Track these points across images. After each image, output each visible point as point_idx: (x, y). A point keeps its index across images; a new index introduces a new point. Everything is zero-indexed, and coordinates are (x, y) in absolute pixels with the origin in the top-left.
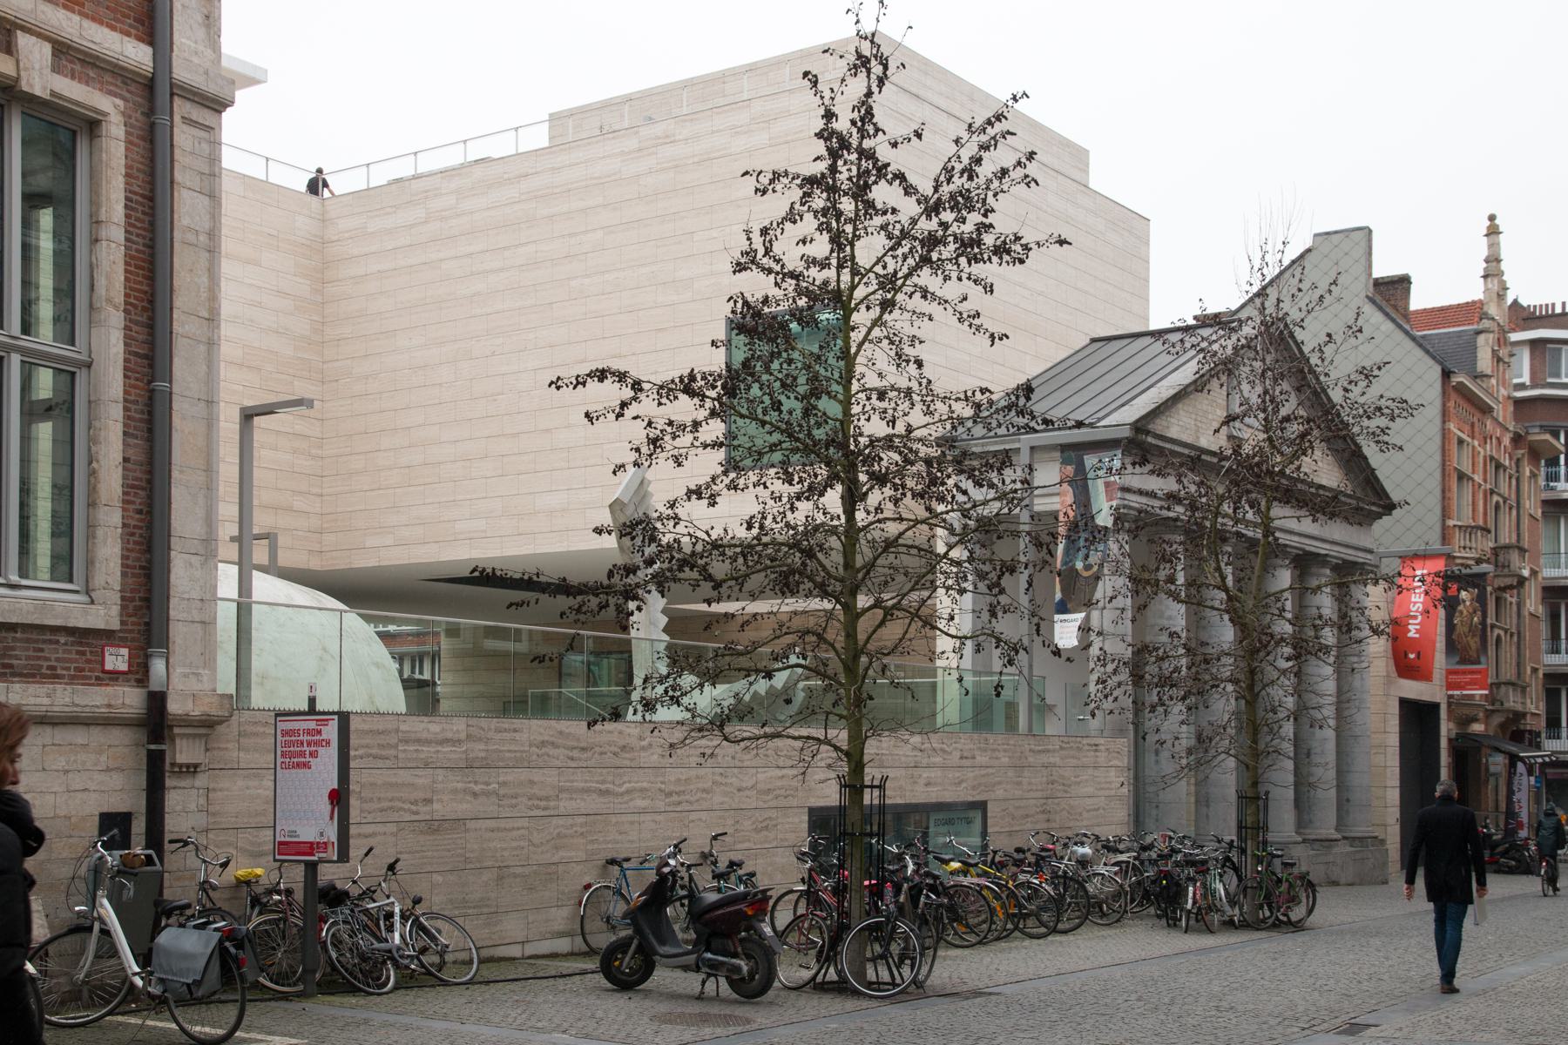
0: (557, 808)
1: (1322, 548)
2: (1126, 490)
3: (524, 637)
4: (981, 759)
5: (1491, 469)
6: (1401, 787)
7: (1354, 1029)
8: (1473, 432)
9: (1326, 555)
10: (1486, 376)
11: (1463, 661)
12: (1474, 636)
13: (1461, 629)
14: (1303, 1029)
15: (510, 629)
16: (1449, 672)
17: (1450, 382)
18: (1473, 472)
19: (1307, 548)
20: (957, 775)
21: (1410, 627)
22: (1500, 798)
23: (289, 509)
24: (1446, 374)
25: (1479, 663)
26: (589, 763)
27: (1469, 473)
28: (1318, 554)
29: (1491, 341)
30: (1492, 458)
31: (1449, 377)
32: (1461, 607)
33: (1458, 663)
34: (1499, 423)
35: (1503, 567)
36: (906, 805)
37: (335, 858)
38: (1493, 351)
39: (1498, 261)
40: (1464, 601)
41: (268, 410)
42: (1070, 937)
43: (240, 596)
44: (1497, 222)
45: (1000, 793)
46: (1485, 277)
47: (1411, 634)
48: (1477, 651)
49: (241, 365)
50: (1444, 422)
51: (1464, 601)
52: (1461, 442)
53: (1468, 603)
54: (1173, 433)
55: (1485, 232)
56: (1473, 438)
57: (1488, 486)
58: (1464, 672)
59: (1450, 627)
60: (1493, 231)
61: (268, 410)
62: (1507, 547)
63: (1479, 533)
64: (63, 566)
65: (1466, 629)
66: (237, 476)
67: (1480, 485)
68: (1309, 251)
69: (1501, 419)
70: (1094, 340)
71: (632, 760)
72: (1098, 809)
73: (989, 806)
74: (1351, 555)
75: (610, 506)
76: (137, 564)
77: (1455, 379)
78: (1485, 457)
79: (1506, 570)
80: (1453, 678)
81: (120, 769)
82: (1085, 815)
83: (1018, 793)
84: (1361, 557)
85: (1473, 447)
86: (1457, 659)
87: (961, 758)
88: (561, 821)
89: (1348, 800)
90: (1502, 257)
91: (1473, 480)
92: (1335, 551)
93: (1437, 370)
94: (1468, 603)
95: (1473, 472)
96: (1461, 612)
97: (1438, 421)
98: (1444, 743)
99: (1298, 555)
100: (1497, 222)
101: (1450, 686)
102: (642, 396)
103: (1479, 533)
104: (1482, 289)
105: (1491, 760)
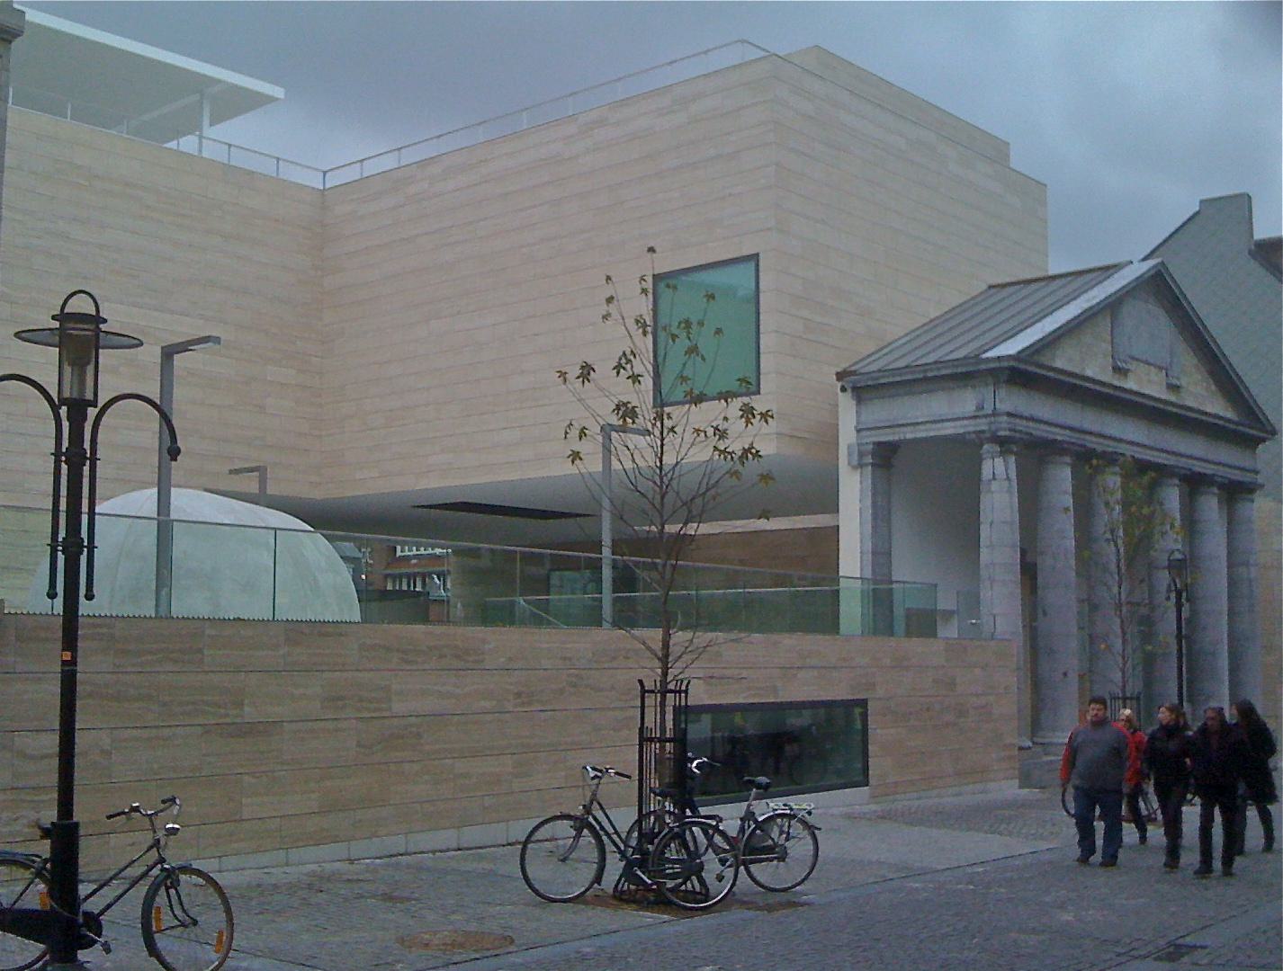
0: (390, 709)
1: (1208, 469)
2: (374, 881)
7: (1175, 952)
9: (1214, 475)
14: (1119, 955)
15: (579, 557)
26: (426, 666)
41: (184, 347)
43: (158, 515)
54: (1059, 364)
61: (184, 347)
68: (1197, 213)
70: (991, 287)
71: (476, 662)
74: (1236, 475)
81: (1205, 521)
84: (1247, 478)
88: (395, 721)
92: (1221, 471)
99: (1185, 475)
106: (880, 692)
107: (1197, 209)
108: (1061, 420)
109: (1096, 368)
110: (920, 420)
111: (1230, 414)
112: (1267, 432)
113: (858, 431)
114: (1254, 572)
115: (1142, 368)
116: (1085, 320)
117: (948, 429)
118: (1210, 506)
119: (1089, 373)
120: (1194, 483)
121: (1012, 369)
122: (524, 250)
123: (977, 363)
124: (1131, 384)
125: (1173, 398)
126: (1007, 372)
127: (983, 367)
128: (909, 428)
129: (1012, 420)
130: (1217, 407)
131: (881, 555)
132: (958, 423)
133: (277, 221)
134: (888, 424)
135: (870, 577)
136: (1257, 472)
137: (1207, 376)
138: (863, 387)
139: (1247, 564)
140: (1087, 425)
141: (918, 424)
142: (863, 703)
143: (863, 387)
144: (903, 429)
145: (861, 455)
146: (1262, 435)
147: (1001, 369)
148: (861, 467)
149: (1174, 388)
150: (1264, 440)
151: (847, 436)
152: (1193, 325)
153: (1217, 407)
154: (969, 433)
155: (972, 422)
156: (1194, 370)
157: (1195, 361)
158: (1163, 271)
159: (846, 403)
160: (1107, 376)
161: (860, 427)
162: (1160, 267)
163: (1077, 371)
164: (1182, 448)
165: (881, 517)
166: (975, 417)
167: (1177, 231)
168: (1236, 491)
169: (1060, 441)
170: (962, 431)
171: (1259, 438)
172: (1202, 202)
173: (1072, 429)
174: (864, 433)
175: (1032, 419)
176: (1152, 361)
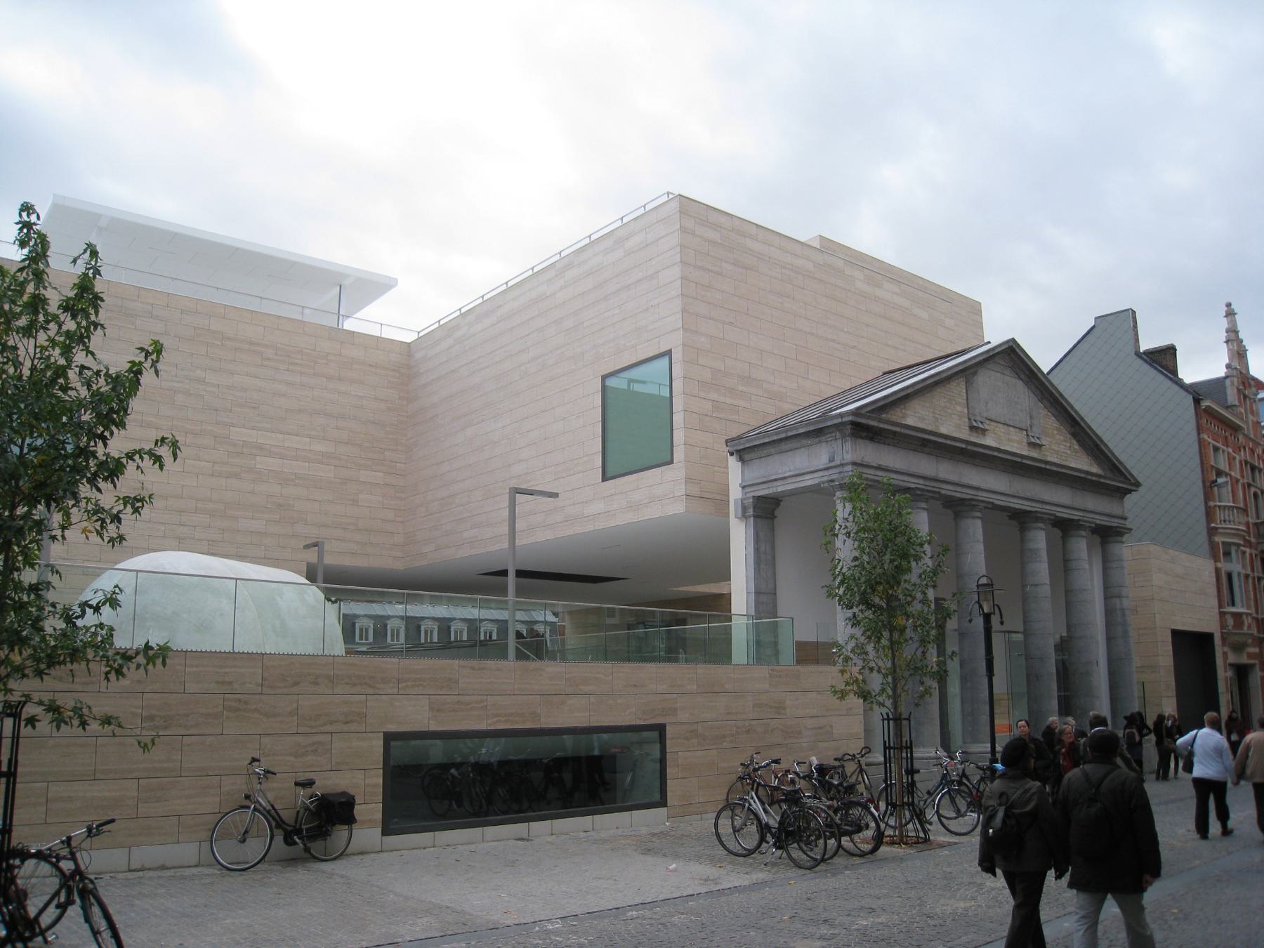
5: (1248, 471)
6: (1177, 696)
8: (1227, 442)
9: (1079, 520)
10: (1235, 406)
18: (1230, 469)
19: (1058, 514)
24: (1197, 401)
27: (1227, 470)
29: (1236, 384)
30: (1246, 462)
31: (1199, 403)
34: (1250, 439)
38: (1239, 390)
39: (1236, 332)
44: (1232, 307)
46: (1227, 342)
50: (1199, 434)
52: (1216, 449)
54: (910, 421)
55: (1225, 314)
56: (1227, 446)
57: (1245, 481)
60: (1230, 314)
63: (1235, 511)
64: (1229, 576)
67: (1237, 481)
69: (1252, 436)
74: (1105, 521)
75: (671, 462)
76: (130, 482)
77: (1205, 404)
84: (1115, 523)
85: (1228, 453)
90: (1239, 328)
91: (1231, 476)
93: (1190, 399)
97: (1195, 433)
103: (1235, 511)
106: (683, 716)
107: (1093, 324)
108: (913, 470)
109: (952, 426)
110: (787, 475)
111: (1095, 469)
112: (1132, 484)
113: (743, 488)
114: (1126, 603)
115: (1001, 429)
116: (937, 383)
117: (809, 481)
118: (1080, 546)
119: (943, 430)
120: (1065, 527)
121: (853, 423)
122: (523, 368)
123: (825, 420)
124: (989, 441)
125: (1034, 454)
126: (850, 426)
127: (829, 423)
128: (779, 483)
129: (860, 469)
130: (1082, 463)
131: (766, 598)
132: (816, 475)
133: (370, 365)
134: (764, 480)
135: (754, 614)
136: (1125, 519)
137: (1069, 436)
138: (745, 450)
139: (1120, 597)
140: (943, 475)
141: (784, 478)
142: (661, 729)
143: (745, 450)
144: (775, 484)
145: (744, 509)
146: (1129, 487)
147: (842, 424)
148: (746, 518)
149: (1033, 445)
150: (1130, 491)
151: (735, 493)
152: (1051, 394)
153: (1082, 463)
154: (823, 483)
155: (826, 473)
156: (1055, 432)
157: (1056, 424)
158: (1014, 346)
159: (734, 464)
160: (964, 434)
161: (744, 484)
162: (1011, 344)
163: (929, 428)
164: (1047, 497)
165: (764, 560)
166: (827, 469)
167: (1079, 342)
168: (1107, 534)
169: (913, 488)
170: (816, 481)
171: (1126, 489)
172: (1096, 318)
173: (924, 478)
174: (747, 490)
175: (879, 468)
176: (1011, 423)
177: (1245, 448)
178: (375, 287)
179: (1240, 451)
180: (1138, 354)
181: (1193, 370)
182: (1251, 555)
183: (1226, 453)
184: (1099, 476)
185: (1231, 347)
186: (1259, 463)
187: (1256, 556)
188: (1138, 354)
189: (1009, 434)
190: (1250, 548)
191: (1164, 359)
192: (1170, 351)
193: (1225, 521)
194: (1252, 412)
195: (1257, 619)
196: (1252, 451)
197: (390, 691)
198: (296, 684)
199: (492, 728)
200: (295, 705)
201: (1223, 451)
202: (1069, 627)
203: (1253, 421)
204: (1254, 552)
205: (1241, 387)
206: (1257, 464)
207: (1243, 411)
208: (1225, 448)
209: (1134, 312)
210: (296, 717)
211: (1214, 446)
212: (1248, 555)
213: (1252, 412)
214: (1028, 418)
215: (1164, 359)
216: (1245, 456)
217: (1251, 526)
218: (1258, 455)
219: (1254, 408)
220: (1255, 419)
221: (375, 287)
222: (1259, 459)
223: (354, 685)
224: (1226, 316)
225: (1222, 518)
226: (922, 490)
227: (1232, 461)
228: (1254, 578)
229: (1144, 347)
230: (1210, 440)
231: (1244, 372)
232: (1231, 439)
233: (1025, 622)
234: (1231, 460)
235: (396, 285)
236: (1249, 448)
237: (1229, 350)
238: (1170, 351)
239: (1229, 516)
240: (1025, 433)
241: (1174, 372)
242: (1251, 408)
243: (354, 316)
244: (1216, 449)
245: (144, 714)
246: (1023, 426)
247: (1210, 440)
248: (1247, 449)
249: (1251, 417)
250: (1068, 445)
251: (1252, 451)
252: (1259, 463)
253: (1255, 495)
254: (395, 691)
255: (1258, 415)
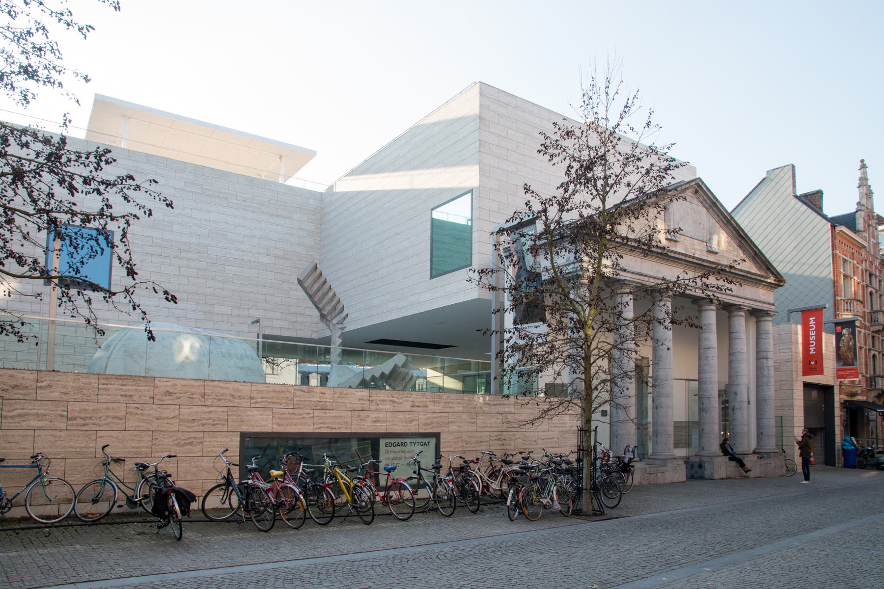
3: (473, 366)
4: (431, 407)
9: (740, 305)
10: (861, 231)
11: (845, 364)
12: (850, 352)
13: (843, 349)
16: (838, 370)
17: (835, 231)
20: (407, 416)
21: (811, 349)
22: (878, 432)
23: (304, 314)
25: (853, 365)
28: (736, 305)
31: (835, 228)
32: (843, 338)
33: (843, 365)
35: (875, 321)
36: (351, 433)
37: (383, 442)
39: (866, 179)
40: (844, 335)
42: (444, 520)
44: (865, 163)
45: (454, 428)
47: (811, 353)
48: (852, 359)
49: (282, 258)
51: (844, 335)
52: (845, 261)
53: (846, 336)
55: (859, 168)
56: (853, 259)
58: (846, 370)
59: (838, 348)
60: (863, 166)
62: (877, 312)
65: (846, 348)
66: (113, 270)
72: (553, 438)
73: (442, 436)
78: (862, 270)
79: (876, 323)
80: (840, 373)
82: (539, 441)
83: (472, 428)
84: (766, 307)
85: (854, 264)
86: (842, 363)
87: (413, 406)
89: (762, 433)
94: (846, 336)
95: (854, 276)
96: (843, 341)
98: (837, 405)
100: (865, 163)
101: (839, 377)
102: (682, 324)
104: (858, 192)
105: (870, 413)
118: (740, 322)
125: (711, 258)
177: (866, 260)
178: (304, 156)
179: (862, 263)
180: (796, 197)
181: (833, 207)
182: (865, 334)
183: (852, 264)
184: (759, 275)
185: (861, 191)
186: (875, 271)
187: (868, 334)
188: (796, 197)
189: (694, 245)
190: (865, 329)
191: (813, 200)
192: (819, 194)
193: (847, 310)
194: (874, 237)
195: (866, 377)
196: (871, 263)
197: (244, 405)
198: (192, 394)
199: (317, 431)
200: (177, 412)
201: (850, 263)
202: (730, 377)
203: (873, 243)
204: (867, 332)
205: (867, 219)
206: (874, 272)
207: (867, 235)
208: (851, 260)
209: (793, 167)
210: (178, 420)
211: (843, 259)
212: (862, 334)
213: (874, 237)
214: (708, 234)
215: (813, 200)
216: (866, 266)
217: (866, 314)
218: (875, 266)
219: (875, 234)
220: (875, 241)
221: (304, 156)
222: (876, 269)
223: (220, 400)
224: (859, 187)
225: (846, 308)
226: (630, 281)
227: (855, 269)
228: (866, 350)
229: (799, 193)
230: (840, 255)
231: (869, 207)
232: (856, 255)
233: (699, 373)
234: (855, 269)
235: (316, 155)
236: (869, 261)
237: (860, 193)
238: (819, 194)
239: (850, 307)
240: (705, 244)
241: (821, 208)
242: (873, 232)
243: (293, 176)
244: (845, 261)
245: (69, 416)
246: (705, 240)
247: (840, 255)
248: (868, 262)
249: (872, 240)
250: (736, 253)
251: (871, 263)
252: (875, 271)
253: (871, 293)
254: (249, 405)
255: (877, 238)
